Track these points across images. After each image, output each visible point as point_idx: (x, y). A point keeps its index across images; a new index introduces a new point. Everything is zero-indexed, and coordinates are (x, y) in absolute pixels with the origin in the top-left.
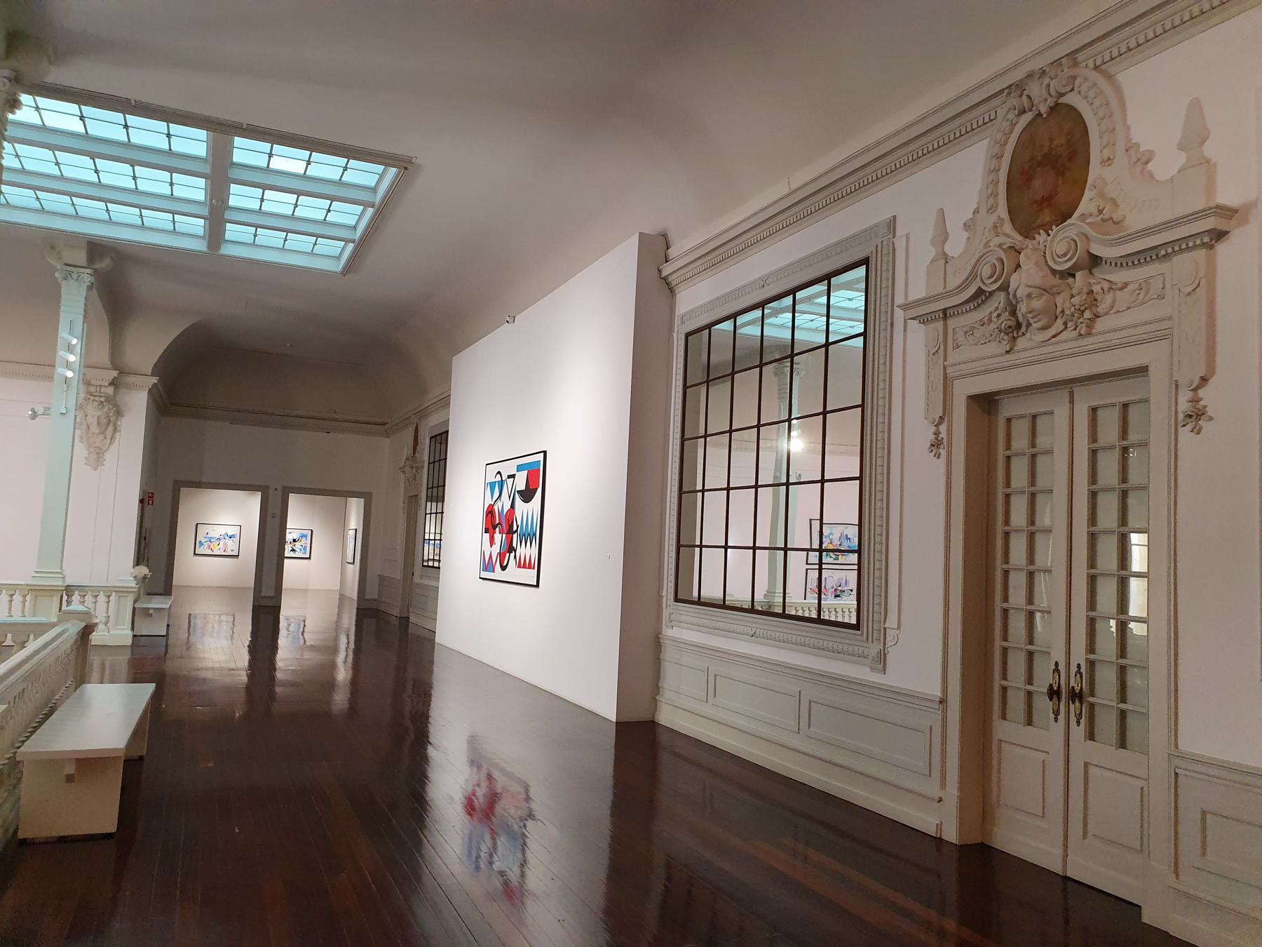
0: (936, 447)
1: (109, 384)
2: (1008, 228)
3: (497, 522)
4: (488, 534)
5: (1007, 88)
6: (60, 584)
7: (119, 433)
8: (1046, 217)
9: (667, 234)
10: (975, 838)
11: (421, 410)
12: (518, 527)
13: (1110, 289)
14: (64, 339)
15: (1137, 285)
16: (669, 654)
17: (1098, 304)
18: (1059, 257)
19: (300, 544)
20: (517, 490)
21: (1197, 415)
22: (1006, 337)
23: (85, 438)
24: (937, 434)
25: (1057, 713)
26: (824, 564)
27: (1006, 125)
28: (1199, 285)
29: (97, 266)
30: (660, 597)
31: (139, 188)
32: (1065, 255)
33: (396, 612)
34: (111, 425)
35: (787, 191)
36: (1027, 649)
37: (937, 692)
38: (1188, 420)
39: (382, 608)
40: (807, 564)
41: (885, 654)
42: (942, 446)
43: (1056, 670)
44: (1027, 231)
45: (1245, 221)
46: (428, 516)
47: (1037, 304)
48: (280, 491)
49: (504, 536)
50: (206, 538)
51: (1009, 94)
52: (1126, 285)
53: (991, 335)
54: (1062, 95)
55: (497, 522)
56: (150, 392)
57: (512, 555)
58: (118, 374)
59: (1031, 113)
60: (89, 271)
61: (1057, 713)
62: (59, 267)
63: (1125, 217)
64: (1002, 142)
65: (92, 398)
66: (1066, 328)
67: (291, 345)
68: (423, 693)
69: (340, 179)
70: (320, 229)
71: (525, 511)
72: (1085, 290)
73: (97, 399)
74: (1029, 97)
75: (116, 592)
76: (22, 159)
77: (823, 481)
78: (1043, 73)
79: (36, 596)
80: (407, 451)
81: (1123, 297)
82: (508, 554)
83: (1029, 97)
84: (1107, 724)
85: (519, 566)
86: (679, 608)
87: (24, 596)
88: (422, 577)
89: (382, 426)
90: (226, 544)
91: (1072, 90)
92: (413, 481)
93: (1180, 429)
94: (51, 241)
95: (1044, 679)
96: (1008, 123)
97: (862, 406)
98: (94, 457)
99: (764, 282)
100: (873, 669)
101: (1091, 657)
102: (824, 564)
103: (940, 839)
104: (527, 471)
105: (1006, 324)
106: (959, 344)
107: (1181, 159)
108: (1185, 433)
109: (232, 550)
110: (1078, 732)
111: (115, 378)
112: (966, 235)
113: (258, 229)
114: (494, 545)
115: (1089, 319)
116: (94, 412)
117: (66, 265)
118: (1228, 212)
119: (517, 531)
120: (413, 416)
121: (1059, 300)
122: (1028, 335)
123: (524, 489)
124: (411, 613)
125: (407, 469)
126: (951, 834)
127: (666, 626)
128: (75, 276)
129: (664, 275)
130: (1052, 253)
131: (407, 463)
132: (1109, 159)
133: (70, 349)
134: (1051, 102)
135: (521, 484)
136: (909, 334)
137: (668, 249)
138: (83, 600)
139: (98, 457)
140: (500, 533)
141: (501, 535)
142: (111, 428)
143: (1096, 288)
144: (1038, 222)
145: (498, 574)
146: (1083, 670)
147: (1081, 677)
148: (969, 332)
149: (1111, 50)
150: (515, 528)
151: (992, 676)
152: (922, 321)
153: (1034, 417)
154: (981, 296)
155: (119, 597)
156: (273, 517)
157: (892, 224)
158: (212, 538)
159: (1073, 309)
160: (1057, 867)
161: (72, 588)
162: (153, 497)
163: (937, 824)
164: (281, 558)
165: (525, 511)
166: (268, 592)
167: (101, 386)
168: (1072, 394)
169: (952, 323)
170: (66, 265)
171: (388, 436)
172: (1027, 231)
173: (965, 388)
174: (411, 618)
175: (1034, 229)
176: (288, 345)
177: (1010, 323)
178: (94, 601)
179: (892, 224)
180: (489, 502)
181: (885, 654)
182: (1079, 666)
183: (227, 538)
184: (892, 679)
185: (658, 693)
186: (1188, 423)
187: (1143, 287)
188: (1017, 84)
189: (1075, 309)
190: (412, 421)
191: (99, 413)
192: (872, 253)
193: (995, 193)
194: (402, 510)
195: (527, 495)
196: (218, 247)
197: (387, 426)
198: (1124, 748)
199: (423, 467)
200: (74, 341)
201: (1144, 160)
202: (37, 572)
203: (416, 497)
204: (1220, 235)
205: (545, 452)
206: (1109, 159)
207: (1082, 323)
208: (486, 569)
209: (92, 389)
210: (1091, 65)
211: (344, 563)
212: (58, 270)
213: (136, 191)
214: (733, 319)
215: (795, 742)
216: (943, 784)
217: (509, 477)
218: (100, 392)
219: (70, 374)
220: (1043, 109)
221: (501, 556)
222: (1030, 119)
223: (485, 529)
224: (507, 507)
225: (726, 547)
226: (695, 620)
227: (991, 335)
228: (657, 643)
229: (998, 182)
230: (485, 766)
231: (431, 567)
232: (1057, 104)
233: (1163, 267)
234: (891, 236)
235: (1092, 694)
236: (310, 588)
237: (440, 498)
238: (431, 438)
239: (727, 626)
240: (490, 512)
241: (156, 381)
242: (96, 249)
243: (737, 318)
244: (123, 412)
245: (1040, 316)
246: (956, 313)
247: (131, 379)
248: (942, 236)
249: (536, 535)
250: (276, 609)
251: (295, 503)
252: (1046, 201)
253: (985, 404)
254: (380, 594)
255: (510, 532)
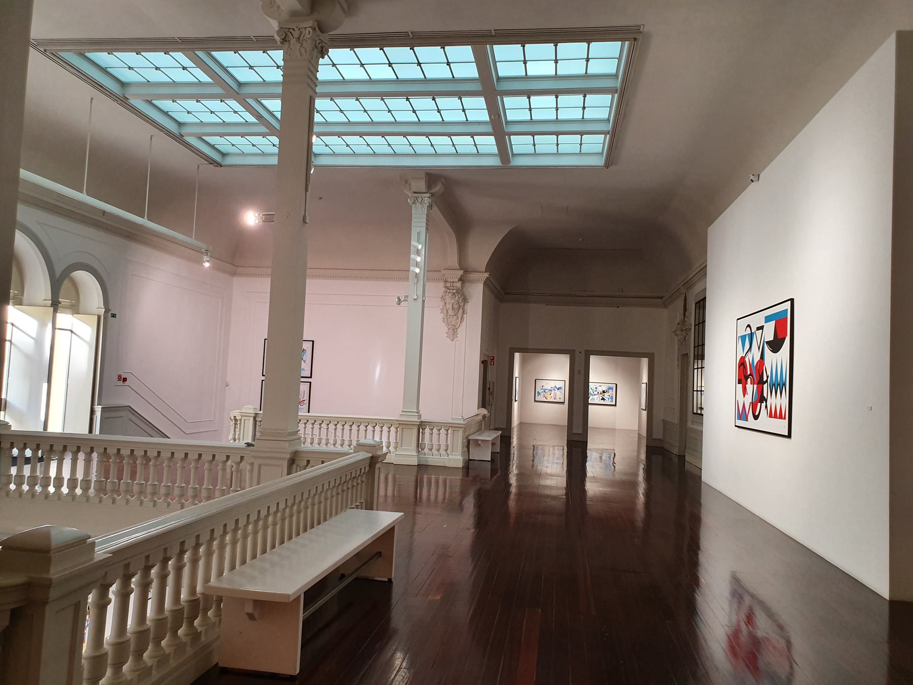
1: (459, 281)
3: (749, 373)
4: (741, 385)
6: (417, 420)
7: (466, 315)
11: (687, 282)
12: (768, 377)
14: (415, 247)
19: (609, 394)
20: (766, 341)
23: (445, 319)
29: (432, 192)
31: (444, 120)
33: (676, 451)
34: (461, 308)
39: (666, 446)
40: (310, 383)
46: (696, 370)
48: (583, 354)
49: (755, 386)
50: (542, 389)
55: (749, 373)
56: (485, 284)
57: (764, 404)
58: (463, 272)
60: (428, 195)
62: (410, 195)
65: (448, 291)
67: (583, 240)
68: (696, 520)
69: (586, 73)
70: (581, 128)
71: (775, 362)
73: (451, 291)
75: (451, 427)
76: (368, 112)
79: (403, 429)
80: (679, 317)
82: (759, 404)
85: (771, 416)
87: (389, 428)
88: (693, 422)
89: (663, 301)
90: (555, 394)
92: (684, 342)
94: (404, 175)
98: (451, 331)
104: (774, 321)
109: (560, 399)
111: (461, 275)
113: (536, 137)
114: (746, 395)
116: (450, 300)
117: (415, 193)
119: (767, 381)
120: (682, 287)
123: (772, 339)
124: (686, 453)
125: (678, 332)
128: (420, 200)
131: (679, 326)
133: (418, 253)
138: (431, 432)
139: (453, 331)
140: (751, 384)
141: (752, 385)
142: (461, 311)
145: (751, 423)
150: (765, 380)
155: (454, 430)
156: (579, 373)
158: (546, 389)
161: (425, 423)
162: (493, 359)
164: (586, 404)
165: (775, 362)
166: (577, 430)
167: (453, 282)
170: (415, 193)
171: (666, 307)
174: (686, 457)
176: (580, 240)
178: (438, 433)
180: (741, 354)
183: (556, 390)
190: (682, 292)
191: (453, 301)
194: (677, 367)
195: (775, 346)
196: (508, 161)
197: (664, 299)
199: (690, 329)
200: (420, 247)
202: (403, 411)
203: (686, 356)
205: (792, 300)
208: (740, 418)
209: (448, 285)
211: (641, 409)
212: (409, 197)
213: (443, 123)
217: (758, 329)
218: (453, 287)
219: (417, 270)
221: (754, 406)
223: (739, 380)
224: (757, 358)
230: (747, 600)
231: (699, 414)
236: (618, 427)
237: (702, 357)
238: (696, 304)
240: (742, 364)
241: (488, 276)
242: (433, 177)
244: (468, 299)
247: (473, 276)
249: (786, 385)
250: (584, 444)
251: (595, 362)
254: (664, 435)
255: (761, 383)
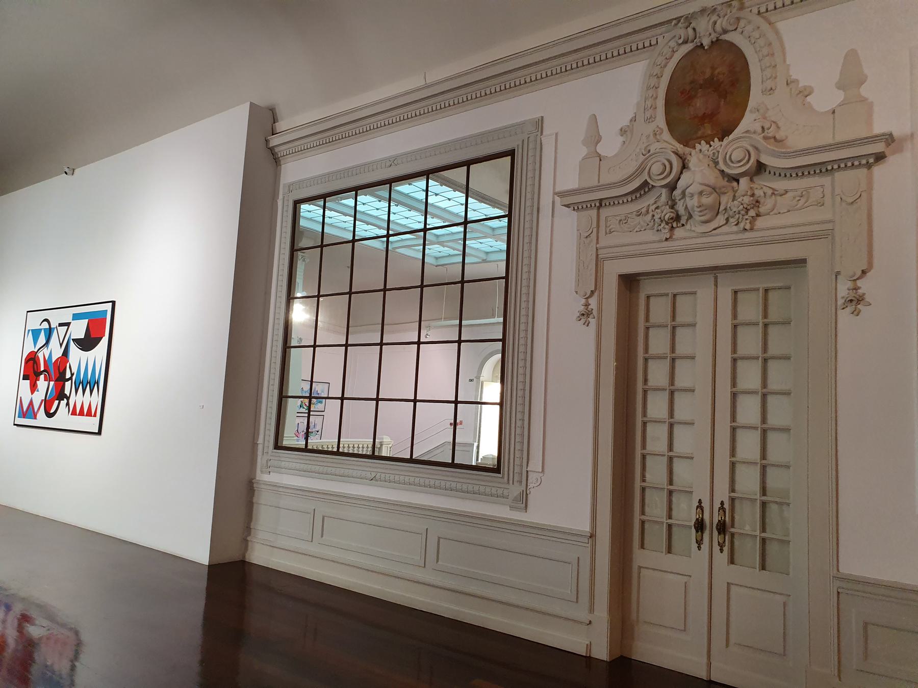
0: (585, 316)
2: (666, 135)
3: (42, 369)
4: (28, 381)
5: (675, 19)
8: (708, 130)
9: (275, 108)
10: (230, 555)
12: (72, 375)
13: (773, 194)
15: (799, 193)
16: (264, 499)
17: (760, 206)
18: (732, 162)
20: (72, 338)
21: (856, 301)
22: (667, 227)
24: (587, 305)
25: (699, 543)
26: (312, 411)
27: (667, 51)
28: (592, 232)
30: (254, 445)
32: (739, 161)
35: (422, 83)
36: (761, 500)
37: (586, 528)
38: (849, 304)
41: (527, 494)
42: (591, 316)
43: (700, 506)
44: (687, 140)
45: (900, 150)
47: (707, 200)
49: (52, 383)
51: (676, 25)
52: (786, 192)
53: (648, 224)
54: (725, 32)
55: (42, 369)
59: (691, 44)
61: (699, 543)
63: (787, 137)
64: (662, 65)
66: (726, 223)
72: (749, 193)
74: (694, 29)
77: (315, 346)
78: (714, 10)
81: (783, 202)
82: (56, 402)
83: (694, 29)
84: (749, 549)
86: (281, 455)
91: (736, 29)
93: (840, 312)
95: (685, 513)
96: (671, 50)
97: (506, 278)
99: (393, 161)
100: (511, 508)
101: (733, 494)
102: (312, 411)
103: (590, 657)
105: (670, 216)
106: (612, 231)
107: (840, 96)
108: (844, 316)
110: (721, 558)
112: (621, 139)
115: (752, 217)
118: (889, 139)
119: (71, 378)
121: (724, 199)
122: (688, 227)
123: (83, 337)
126: (601, 652)
127: (262, 472)
129: (271, 145)
130: (725, 157)
132: (771, 89)
134: (714, 37)
135: (79, 330)
136: (556, 219)
137: (274, 123)
143: (759, 193)
144: (700, 133)
146: (726, 506)
147: (725, 512)
148: (624, 221)
149: (546, 71)
150: (68, 375)
151: (632, 511)
152: (576, 208)
153: (675, 296)
154: (645, 188)
157: (539, 123)
159: (742, 207)
160: (703, 675)
163: (587, 645)
168: (716, 278)
169: (605, 212)
172: (687, 140)
173: (614, 270)
175: (698, 138)
177: (672, 215)
179: (539, 123)
180: (30, 348)
181: (527, 494)
182: (722, 503)
184: (533, 516)
185: (249, 534)
186: (847, 307)
187: (804, 194)
188: (687, 17)
189: (744, 207)
192: (518, 146)
193: (654, 107)
198: (733, 564)
201: (806, 93)
204: (880, 157)
205: (114, 303)
206: (771, 89)
207: (747, 219)
208: (24, 415)
210: (755, 10)
214: (466, 167)
215: (419, 575)
216: (591, 610)
217: (61, 325)
220: (706, 42)
221: (47, 404)
222: (690, 49)
225: (342, 399)
226: (298, 466)
227: (648, 224)
228: (251, 487)
229: (657, 97)
232: (718, 40)
233: (826, 180)
234: (539, 133)
235: (733, 526)
239: (342, 471)
243: (471, 166)
245: (707, 211)
246: (612, 204)
248: (594, 138)
252: (708, 117)
253: (629, 282)
255: (61, 379)
